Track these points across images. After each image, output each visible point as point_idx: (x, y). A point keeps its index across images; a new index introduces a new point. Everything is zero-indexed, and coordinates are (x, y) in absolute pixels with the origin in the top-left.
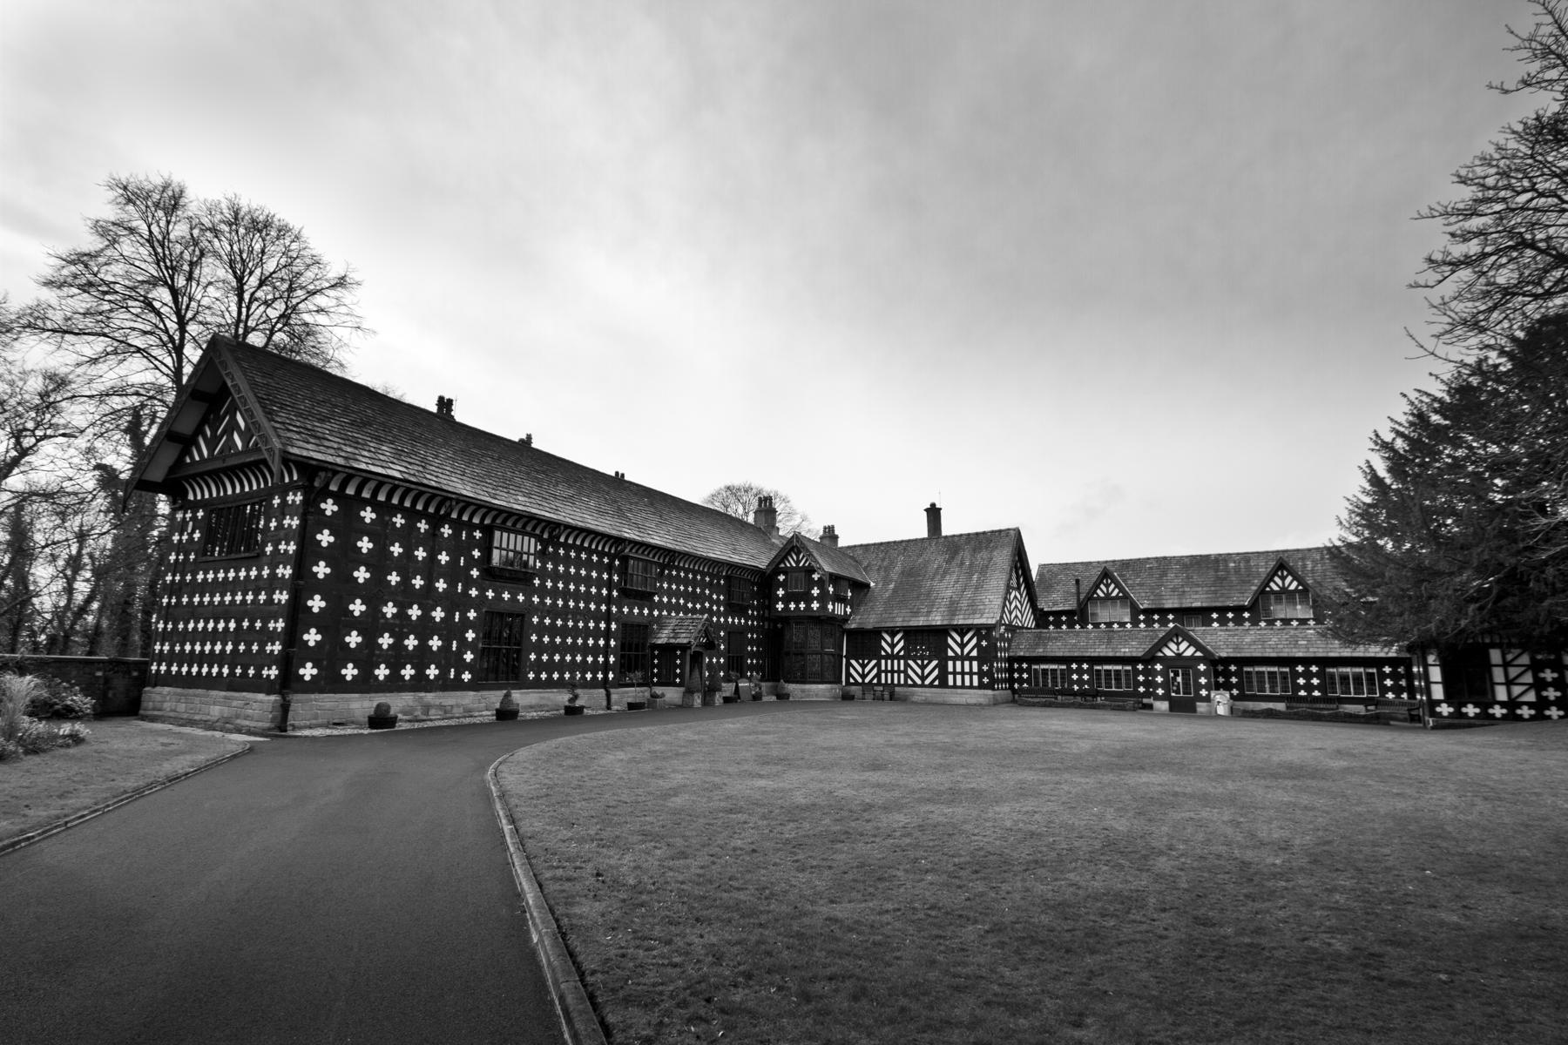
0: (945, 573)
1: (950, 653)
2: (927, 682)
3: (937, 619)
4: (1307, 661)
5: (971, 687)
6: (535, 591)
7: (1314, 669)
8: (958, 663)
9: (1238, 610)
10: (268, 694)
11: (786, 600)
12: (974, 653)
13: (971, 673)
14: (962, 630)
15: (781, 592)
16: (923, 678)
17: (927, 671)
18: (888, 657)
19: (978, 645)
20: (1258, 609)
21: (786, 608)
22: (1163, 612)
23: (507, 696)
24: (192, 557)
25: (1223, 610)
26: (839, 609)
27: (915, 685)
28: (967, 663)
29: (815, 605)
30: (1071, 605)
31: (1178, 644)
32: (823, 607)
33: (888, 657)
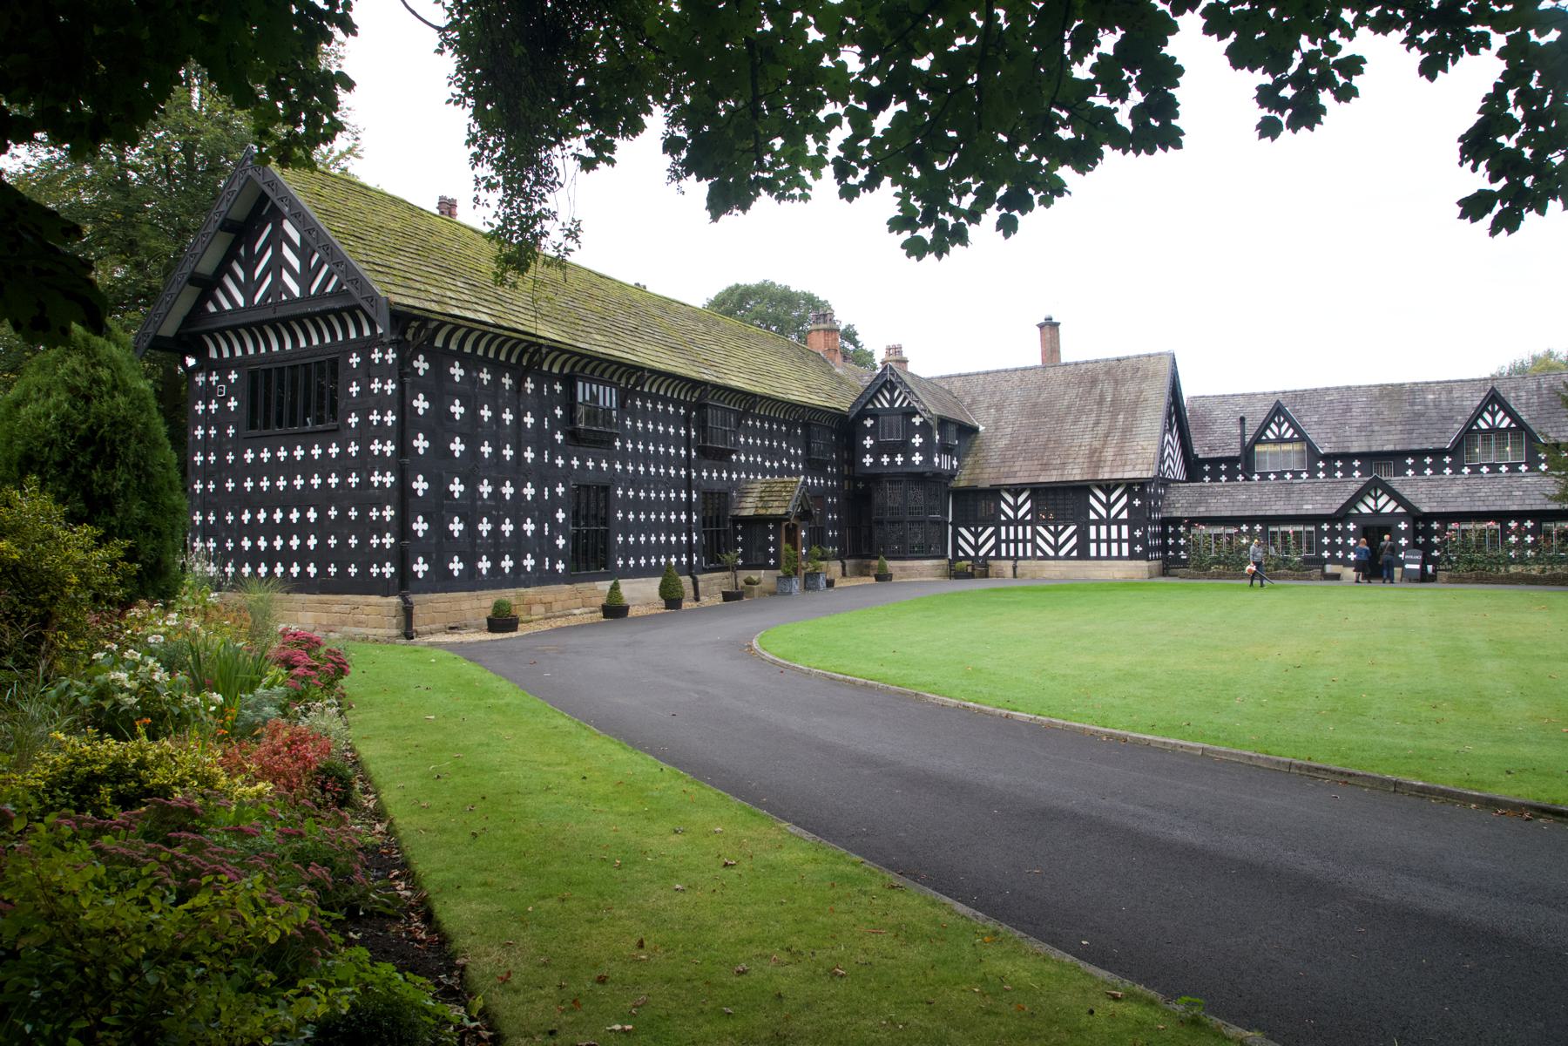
0: (1081, 411)
1: (1093, 516)
2: (1062, 553)
3: (1075, 474)
4: (1521, 516)
5: (1120, 557)
7: (1529, 524)
8: (1103, 529)
9: (1438, 454)
10: (386, 595)
11: (877, 452)
12: (1124, 515)
13: (1120, 541)
14: (1108, 487)
15: (868, 442)
16: (1056, 548)
17: (1061, 539)
18: (1009, 523)
19: (1128, 505)
20: (1458, 453)
22: (1347, 457)
23: (615, 588)
24: (231, 431)
25: (1419, 454)
26: (942, 462)
27: (1046, 557)
28: (1114, 528)
29: (917, 458)
30: (1234, 450)
31: (1376, 499)
33: (1009, 523)
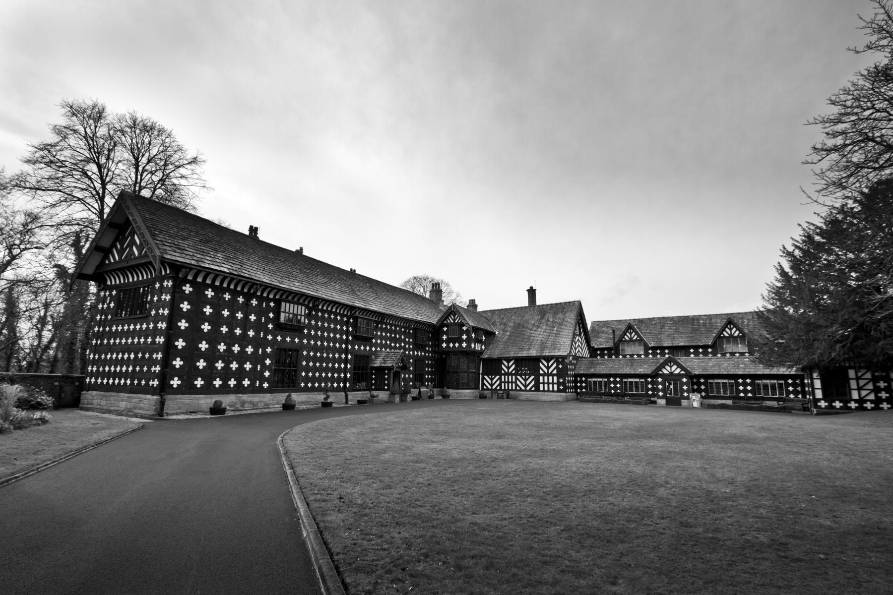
0: (538, 326)
1: (541, 372)
2: (528, 388)
3: (534, 353)
4: (744, 377)
5: (553, 391)
6: (305, 336)
7: (748, 381)
8: (546, 378)
9: (705, 347)
10: (153, 395)
11: (448, 341)
12: (555, 372)
13: (553, 383)
14: (548, 359)
15: (445, 337)
16: (526, 386)
17: (528, 382)
18: (505, 374)
19: (557, 367)
20: (716, 347)
21: (448, 346)
22: (663, 348)
23: (289, 396)
24: (109, 317)
25: (696, 348)
26: (478, 347)
27: (521, 390)
28: (551, 378)
29: (464, 345)
30: (610, 344)
31: (671, 367)
32: (469, 346)
33: (505, 374)
